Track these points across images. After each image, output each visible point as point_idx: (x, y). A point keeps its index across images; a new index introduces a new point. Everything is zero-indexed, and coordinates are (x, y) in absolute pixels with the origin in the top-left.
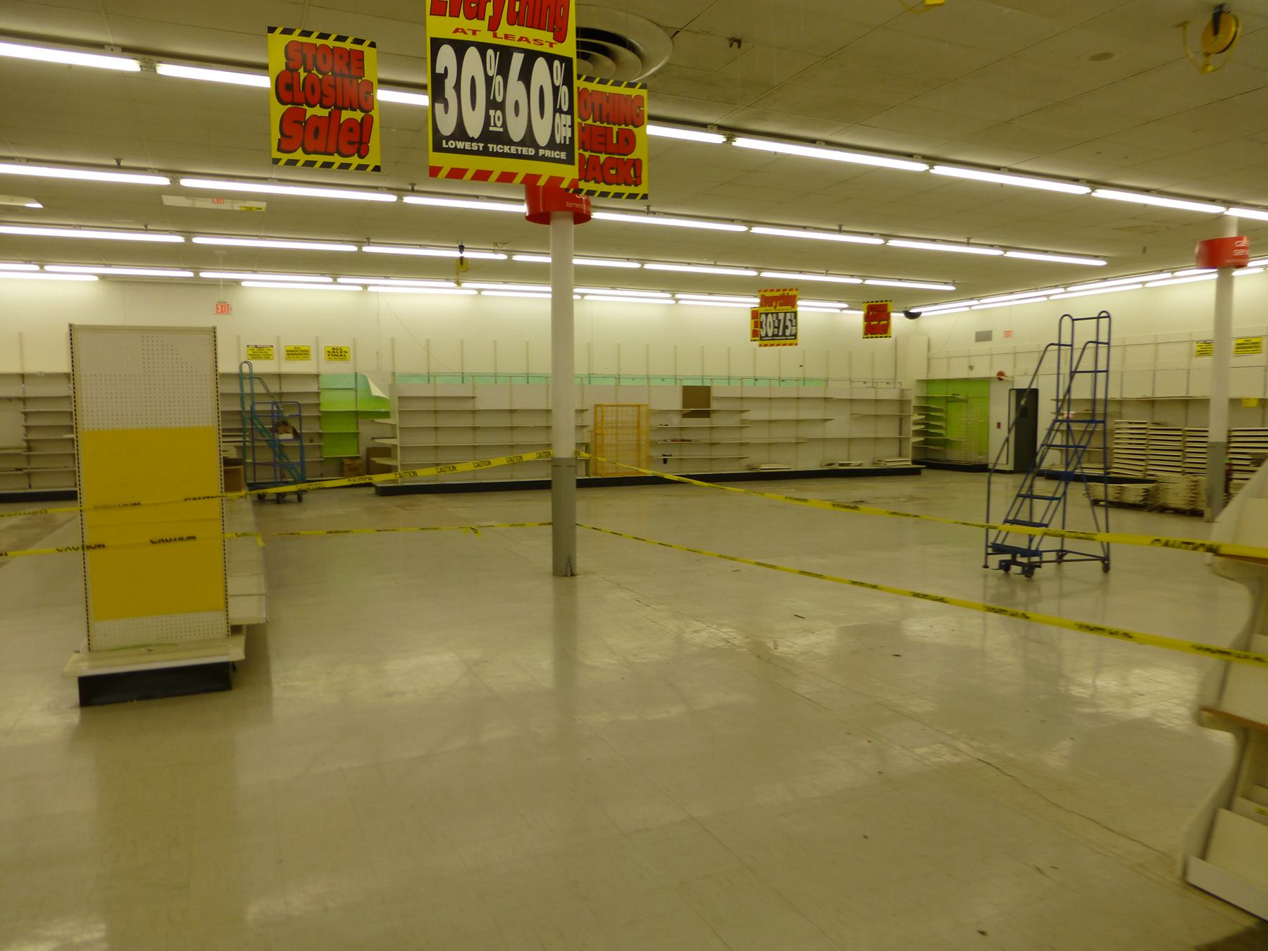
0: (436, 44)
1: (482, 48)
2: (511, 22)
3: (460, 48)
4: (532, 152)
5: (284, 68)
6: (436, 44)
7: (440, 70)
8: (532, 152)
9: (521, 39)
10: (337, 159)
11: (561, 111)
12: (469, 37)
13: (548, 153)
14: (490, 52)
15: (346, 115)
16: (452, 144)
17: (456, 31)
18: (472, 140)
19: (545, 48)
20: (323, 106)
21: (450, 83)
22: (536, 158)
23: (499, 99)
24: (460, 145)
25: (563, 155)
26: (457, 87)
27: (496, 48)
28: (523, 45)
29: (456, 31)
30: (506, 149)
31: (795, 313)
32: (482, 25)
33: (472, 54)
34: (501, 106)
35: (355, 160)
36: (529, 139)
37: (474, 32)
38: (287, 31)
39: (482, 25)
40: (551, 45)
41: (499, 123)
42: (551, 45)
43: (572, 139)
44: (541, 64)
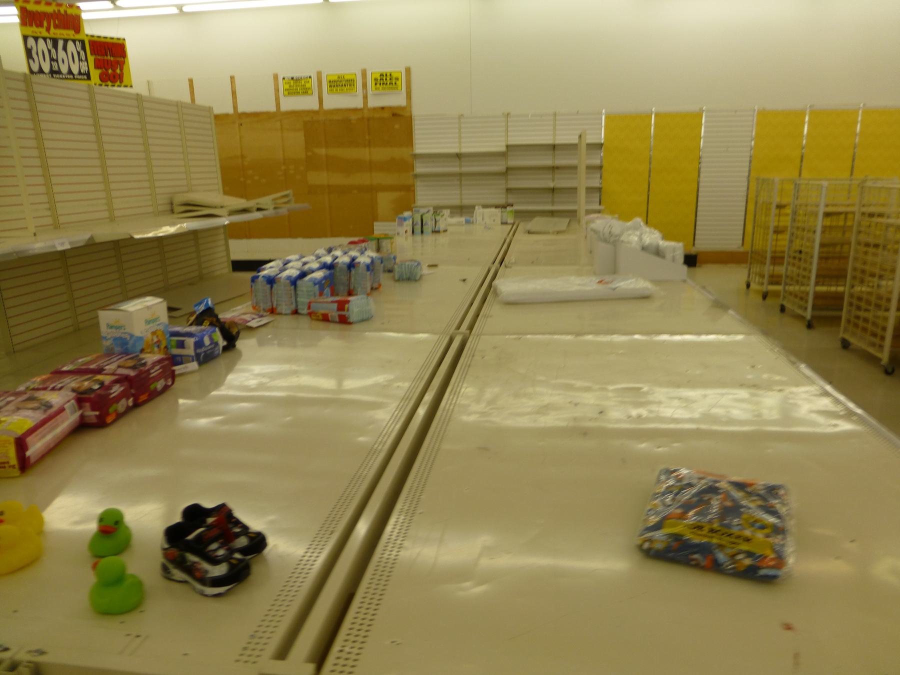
1: (45, 39)
19: (72, 37)
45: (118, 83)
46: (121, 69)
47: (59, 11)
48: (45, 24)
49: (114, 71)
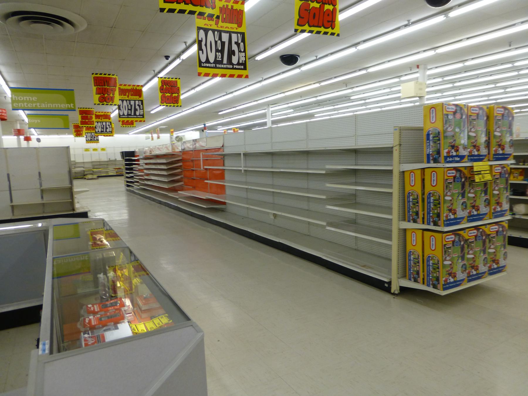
1: (126, 100)
2: (222, 22)
4: (231, 67)
6: (199, 28)
8: (231, 67)
9: (226, 28)
10: (172, 105)
11: (241, 52)
12: (209, 27)
13: (237, 67)
14: (216, 32)
15: (174, 95)
16: (205, 65)
17: (205, 25)
18: (211, 63)
19: (235, 30)
21: (203, 43)
22: (233, 68)
24: (207, 65)
25: (242, 67)
26: (206, 45)
27: (218, 31)
29: (205, 25)
30: (223, 66)
31: (142, 101)
32: (126, 97)
33: (125, 102)
35: (176, 105)
37: (211, 25)
39: (126, 97)
40: (237, 29)
41: (220, 57)
42: (237, 29)
43: (245, 61)
47: (227, 6)
48: (127, 94)
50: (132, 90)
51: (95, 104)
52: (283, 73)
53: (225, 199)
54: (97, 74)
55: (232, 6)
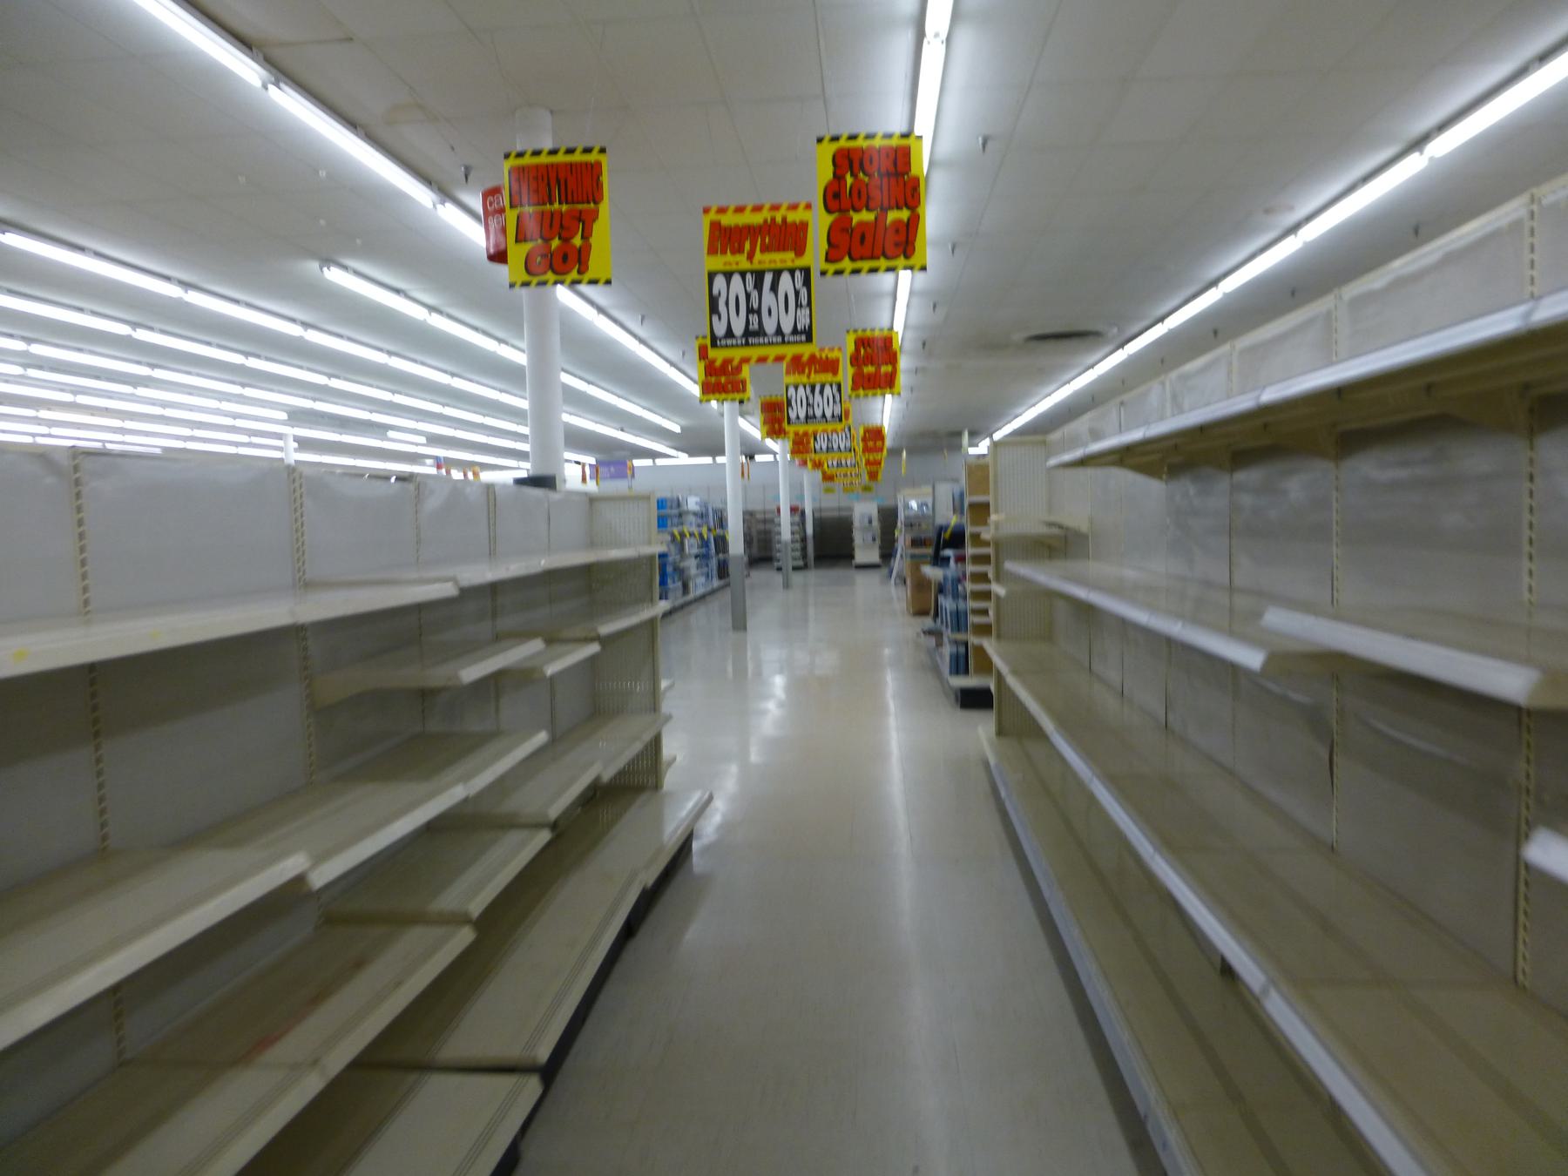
0: (712, 276)
2: (763, 250)
3: (728, 276)
5: (830, 176)
7: (715, 292)
12: (734, 267)
20: (868, 209)
23: (756, 306)
24: (729, 342)
26: (727, 304)
28: (773, 266)
33: (736, 279)
34: (759, 312)
36: (779, 331)
38: (835, 139)
44: (785, 277)
45: (574, 275)
46: (586, 236)
47: (773, 220)
48: (747, 246)
49: (566, 240)
50: (768, 228)
51: (608, 282)
52: (1367, 178)
53: (1085, 445)
54: (520, 155)
55: (784, 220)
